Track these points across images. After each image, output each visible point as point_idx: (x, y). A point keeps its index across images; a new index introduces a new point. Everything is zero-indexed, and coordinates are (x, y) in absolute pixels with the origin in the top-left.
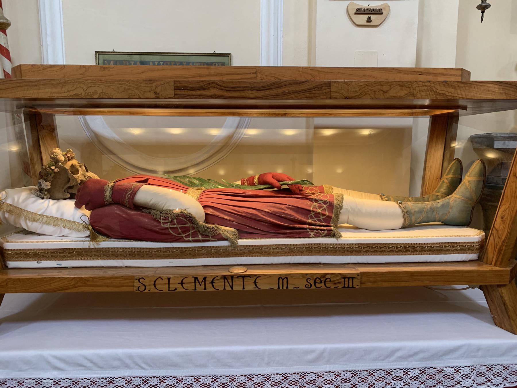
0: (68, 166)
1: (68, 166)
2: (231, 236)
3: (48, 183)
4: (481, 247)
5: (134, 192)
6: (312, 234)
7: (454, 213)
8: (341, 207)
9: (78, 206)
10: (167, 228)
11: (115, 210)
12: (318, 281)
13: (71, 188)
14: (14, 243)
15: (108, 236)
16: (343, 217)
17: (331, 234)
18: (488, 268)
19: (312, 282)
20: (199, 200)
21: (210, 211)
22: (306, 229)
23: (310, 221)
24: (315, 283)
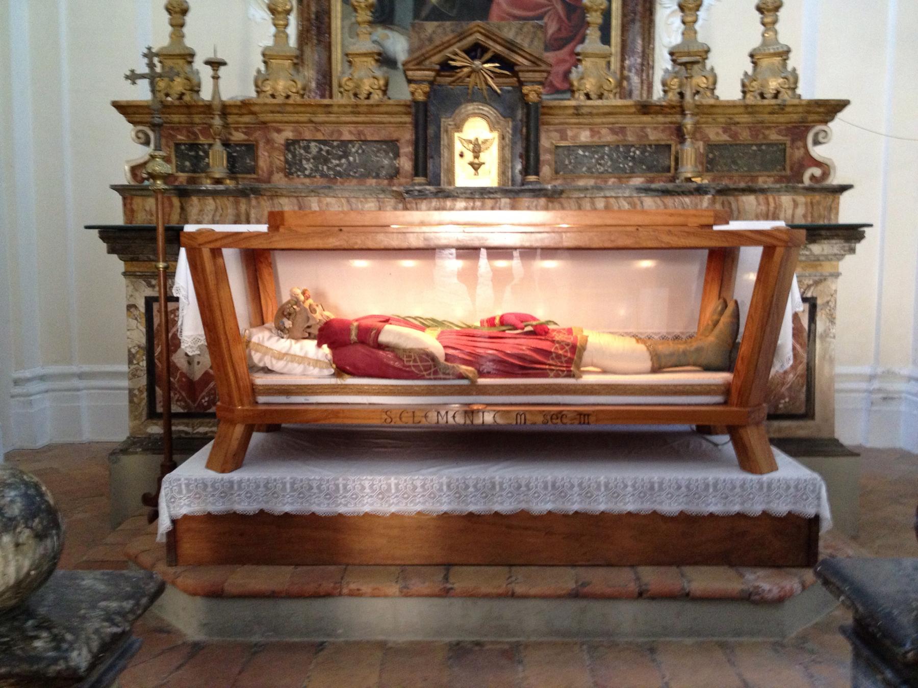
0: (307, 305)
1: (307, 305)
2: (471, 375)
3: (290, 322)
4: (726, 390)
5: (379, 332)
6: (552, 374)
7: (710, 357)
8: (584, 348)
9: (319, 345)
10: (409, 366)
11: (361, 349)
12: (554, 417)
13: (309, 327)
14: (261, 380)
15: (353, 374)
16: (587, 357)
17: (570, 375)
18: (734, 409)
19: (549, 417)
20: (439, 338)
21: (451, 351)
22: (545, 369)
23: (551, 362)
24: (551, 419)
